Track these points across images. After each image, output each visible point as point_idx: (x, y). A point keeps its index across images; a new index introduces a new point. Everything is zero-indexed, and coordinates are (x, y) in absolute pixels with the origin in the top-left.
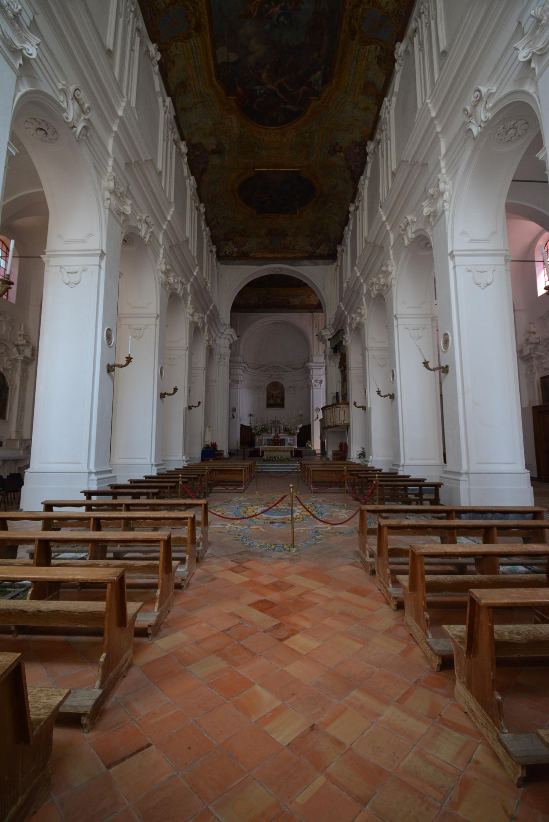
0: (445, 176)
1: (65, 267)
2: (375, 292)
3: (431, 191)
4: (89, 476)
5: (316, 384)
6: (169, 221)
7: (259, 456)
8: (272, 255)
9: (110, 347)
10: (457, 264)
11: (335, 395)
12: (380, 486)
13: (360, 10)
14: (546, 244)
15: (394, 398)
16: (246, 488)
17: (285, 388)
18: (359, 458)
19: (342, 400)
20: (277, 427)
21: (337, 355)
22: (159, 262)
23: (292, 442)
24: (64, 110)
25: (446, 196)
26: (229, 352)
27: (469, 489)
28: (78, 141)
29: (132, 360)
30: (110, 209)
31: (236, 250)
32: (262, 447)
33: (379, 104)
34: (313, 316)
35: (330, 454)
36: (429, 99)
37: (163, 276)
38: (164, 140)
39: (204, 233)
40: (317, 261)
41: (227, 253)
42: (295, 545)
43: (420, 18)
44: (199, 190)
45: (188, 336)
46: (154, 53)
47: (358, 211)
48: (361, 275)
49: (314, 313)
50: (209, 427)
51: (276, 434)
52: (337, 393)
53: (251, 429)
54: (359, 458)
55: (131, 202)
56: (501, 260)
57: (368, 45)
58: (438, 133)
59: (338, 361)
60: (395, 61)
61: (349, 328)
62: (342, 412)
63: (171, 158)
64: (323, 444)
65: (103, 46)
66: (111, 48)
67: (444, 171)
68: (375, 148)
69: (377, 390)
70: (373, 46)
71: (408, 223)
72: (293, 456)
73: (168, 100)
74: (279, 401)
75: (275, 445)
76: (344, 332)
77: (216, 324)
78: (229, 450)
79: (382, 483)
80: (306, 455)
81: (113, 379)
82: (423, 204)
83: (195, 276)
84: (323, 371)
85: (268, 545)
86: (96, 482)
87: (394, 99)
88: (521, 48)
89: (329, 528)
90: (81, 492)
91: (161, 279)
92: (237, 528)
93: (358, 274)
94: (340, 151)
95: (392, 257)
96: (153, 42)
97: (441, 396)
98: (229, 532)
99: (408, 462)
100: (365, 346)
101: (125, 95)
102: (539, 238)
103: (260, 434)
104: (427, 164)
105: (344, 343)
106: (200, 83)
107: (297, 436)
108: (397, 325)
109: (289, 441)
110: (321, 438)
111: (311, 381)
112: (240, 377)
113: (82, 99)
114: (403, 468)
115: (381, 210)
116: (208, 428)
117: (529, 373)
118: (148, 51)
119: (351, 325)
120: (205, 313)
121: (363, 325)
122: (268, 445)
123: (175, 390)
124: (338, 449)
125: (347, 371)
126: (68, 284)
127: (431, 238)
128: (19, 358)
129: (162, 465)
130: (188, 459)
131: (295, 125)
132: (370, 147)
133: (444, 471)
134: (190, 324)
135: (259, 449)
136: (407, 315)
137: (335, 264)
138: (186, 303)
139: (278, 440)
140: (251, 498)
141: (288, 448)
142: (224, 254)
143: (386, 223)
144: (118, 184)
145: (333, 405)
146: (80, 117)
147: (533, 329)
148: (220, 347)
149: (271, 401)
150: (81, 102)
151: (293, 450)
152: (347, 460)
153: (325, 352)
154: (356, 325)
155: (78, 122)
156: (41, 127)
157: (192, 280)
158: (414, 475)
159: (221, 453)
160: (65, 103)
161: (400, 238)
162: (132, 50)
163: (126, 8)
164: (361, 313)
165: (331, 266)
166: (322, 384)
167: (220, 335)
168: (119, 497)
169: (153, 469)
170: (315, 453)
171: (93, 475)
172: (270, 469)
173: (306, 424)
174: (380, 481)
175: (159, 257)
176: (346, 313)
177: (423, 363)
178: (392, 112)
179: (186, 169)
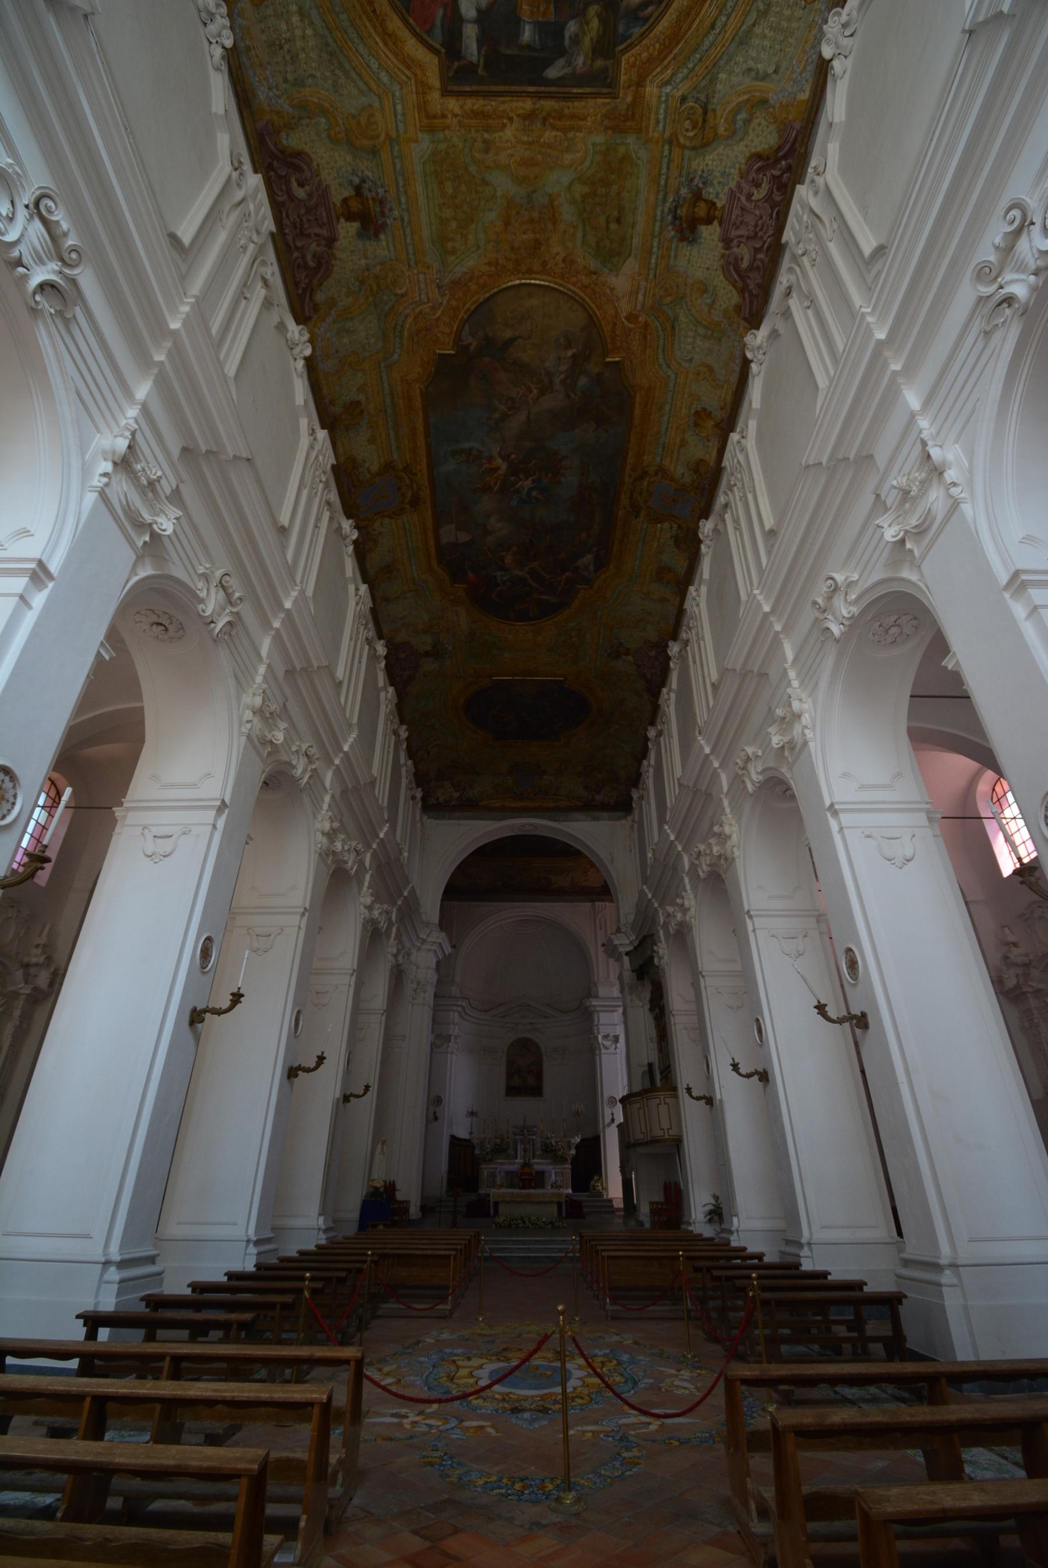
0: (799, 690)
1: (150, 827)
2: (754, 777)
3: (779, 712)
4: (104, 1271)
6: (288, 612)
8: (519, 804)
9: (204, 973)
11: (646, 1068)
12: (765, 1303)
13: (645, 483)
14: (994, 790)
15: (767, 1080)
19: (661, 1080)
22: (320, 818)
24: (201, 601)
25: (806, 719)
27: (965, 1308)
28: (215, 640)
29: (242, 999)
30: (249, 737)
31: (457, 795)
33: (683, 594)
35: (644, 1209)
37: (325, 840)
38: (351, 639)
39: (404, 770)
40: (597, 814)
41: (441, 800)
42: (573, 1480)
43: (731, 491)
44: (400, 707)
45: (357, 947)
46: (348, 531)
47: (662, 738)
48: (677, 838)
49: (597, 903)
50: (383, 1143)
52: (650, 1065)
53: (473, 1147)
54: (710, 1221)
55: (286, 725)
56: (922, 819)
57: (660, 523)
58: (777, 633)
59: (647, 995)
60: (700, 542)
61: (664, 934)
62: (663, 1108)
63: (360, 662)
65: (275, 521)
66: (286, 524)
67: (795, 684)
68: (681, 651)
69: (731, 1062)
70: (666, 525)
71: (748, 757)
72: (564, 1215)
73: (364, 588)
75: (523, 1187)
78: (422, 1200)
79: (767, 1295)
81: (197, 1038)
82: (770, 730)
83: (382, 840)
84: (617, 1016)
85: (505, 1481)
86: (116, 1286)
87: (704, 589)
88: (773, 733)
89: (653, 1427)
90: (78, 1317)
91: (319, 846)
92: (430, 1426)
93: (672, 837)
94: (627, 654)
95: (728, 810)
96: (348, 517)
97: (863, 1072)
98: (411, 1437)
99: (819, 1235)
100: (697, 968)
101: (298, 581)
102: (980, 778)
103: (491, 1160)
104: (711, 794)
105: (656, 960)
107: (572, 1164)
108: (754, 930)
109: (553, 1176)
111: (596, 1038)
113: (231, 587)
114: (811, 1250)
115: (700, 738)
116: (379, 1146)
117: (1026, 1025)
118: (340, 528)
120: (394, 903)
121: (690, 928)
122: (507, 1188)
123: (321, 1059)
126: (150, 856)
127: (792, 782)
128: (22, 991)
129: (268, 1240)
130: (331, 1224)
132: (674, 649)
133: (902, 1259)
134: (363, 924)
135: (488, 1195)
136: (769, 910)
137: (629, 818)
142: (435, 802)
143: (712, 757)
144: (269, 700)
145: (644, 1093)
146: (224, 609)
147: (1011, 938)
148: (418, 968)
150: (230, 591)
151: (563, 1200)
152: (683, 1227)
153: (620, 978)
154: (676, 927)
155: (219, 616)
156: (160, 621)
157: (374, 846)
158: (840, 1271)
159: (404, 1207)
160: (205, 592)
161: (738, 781)
162: (316, 526)
163: (314, 478)
164: (682, 905)
165: (623, 822)
166: (618, 1045)
168: (161, 1333)
170: (612, 1206)
171: (113, 1269)
174: (764, 1289)
175: (321, 808)
176: (656, 905)
177: (816, 1007)
178: (703, 605)
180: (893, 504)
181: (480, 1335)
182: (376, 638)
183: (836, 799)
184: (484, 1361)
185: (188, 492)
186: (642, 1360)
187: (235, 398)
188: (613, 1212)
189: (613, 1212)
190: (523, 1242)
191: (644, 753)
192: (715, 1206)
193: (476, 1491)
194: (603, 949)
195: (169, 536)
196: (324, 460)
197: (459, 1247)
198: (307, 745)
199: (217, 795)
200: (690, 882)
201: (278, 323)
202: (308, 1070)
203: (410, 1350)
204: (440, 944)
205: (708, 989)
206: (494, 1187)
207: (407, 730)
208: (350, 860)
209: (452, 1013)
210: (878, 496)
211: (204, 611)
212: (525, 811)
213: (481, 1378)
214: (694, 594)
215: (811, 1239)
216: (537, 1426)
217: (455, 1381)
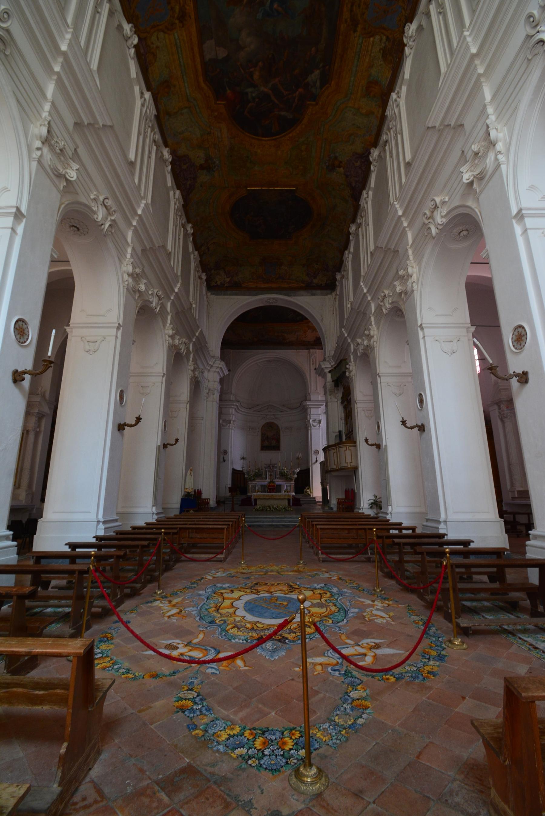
2: (388, 306)
3: (401, 272)
6: (140, 216)
7: (251, 504)
8: (267, 286)
10: (426, 334)
15: (424, 430)
16: (229, 553)
17: (281, 429)
18: (371, 508)
20: (273, 472)
21: (338, 390)
22: (125, 263)
23: (289, 489)
26: (219, 387)
28: (105, 236)
30: (127, 289)
31: (228, 280)
32: (254, 495)
34: (309, 352)
35: (334, 502)
36: (468, 31)
38: (173, 225)
40: (314, 292)
41: (219, 283)
48: (368, 291)
49: (311, 350)
50: (191, 470)
51: (271, 479)
52: (340, 432)
53: (244, 474)
54: (371, 508)
57: (372, 36)
58: (405, 228)
59: (340, 395)
60: (370, 163)
62: (348, 452)
64: (324, 491)
68: (356, 230)
70: (377, 37)
73: (178, 192)
75: (270, 492)
76: (347, 362)
77: (203, 354)
82: (395, 283)
83: (176, 293)
88: (464, 172)
90: (66, 544)
93: (365, 291)
96: (129, 22)
99: (452, 517)
101: (70, 20)
103: (253, 480)
104: (398, 251)
105: (347, 374)
106: (186, 84)
107: (295, 481)
109: (285, 487)
112: (233, 417)
116: (189, 472)
119: (357, 352)
122: (262, 492)
123: (177, 440)
124: (344, 497)
125: (352, 406)
129: (161, 513)
130: (161, 511)
131: (290, 135)
134: (191, 379)
135: (252, 496)
137: (334, 294)
139: (274, 486)
140: (232, 571)
141: (285, 495)
142: (216, 284)
143: (403, 219)
148: (209, 381)
151: (291, 498)
152: (356, 510)
153: (325, 387)
157: (172, 298)
159: (206, 502)
163: (145, 126)
164: (369, 335)
165: (329, 296)
166: (321, 425)
167: (209, 368)
168: (78, 561)
169: (98, 527)
170: (315, 500)
172: (263, 522)
173: (304, 468)
175: (126, 256)
178: (370, 203)
179: (134, 66)
180: (469, 159)
181: (241, 573)
182: (187, 223)
183: (424, 322)
184: (242, 593)
185: (82, 151)
186: (346, 593)
187: (99, 87)
189: (316, 503)
190: (269, 518)
191: (346, 246)
192: (374, 500)
193: (218, 751)
194: (315, 371)
195: (75, 181)
196: (150, 113)
197: (231, 523)
198: (157, 290)
199: (14, 203)
200: (374, 320)
201: (118, 25)
202: (172, 445)
203: (195, 585)
205: (382, 383)
206: (255, 492)
207: (206, 275)
208: (183, 349)
209: (231, 409)
210: (463, 152)
211: (97, 218)
212: (270, 290)
213: (239, 608)
214: (365, 196)
215: (447, 519)
216: (276, 658)
217: (220, 611)
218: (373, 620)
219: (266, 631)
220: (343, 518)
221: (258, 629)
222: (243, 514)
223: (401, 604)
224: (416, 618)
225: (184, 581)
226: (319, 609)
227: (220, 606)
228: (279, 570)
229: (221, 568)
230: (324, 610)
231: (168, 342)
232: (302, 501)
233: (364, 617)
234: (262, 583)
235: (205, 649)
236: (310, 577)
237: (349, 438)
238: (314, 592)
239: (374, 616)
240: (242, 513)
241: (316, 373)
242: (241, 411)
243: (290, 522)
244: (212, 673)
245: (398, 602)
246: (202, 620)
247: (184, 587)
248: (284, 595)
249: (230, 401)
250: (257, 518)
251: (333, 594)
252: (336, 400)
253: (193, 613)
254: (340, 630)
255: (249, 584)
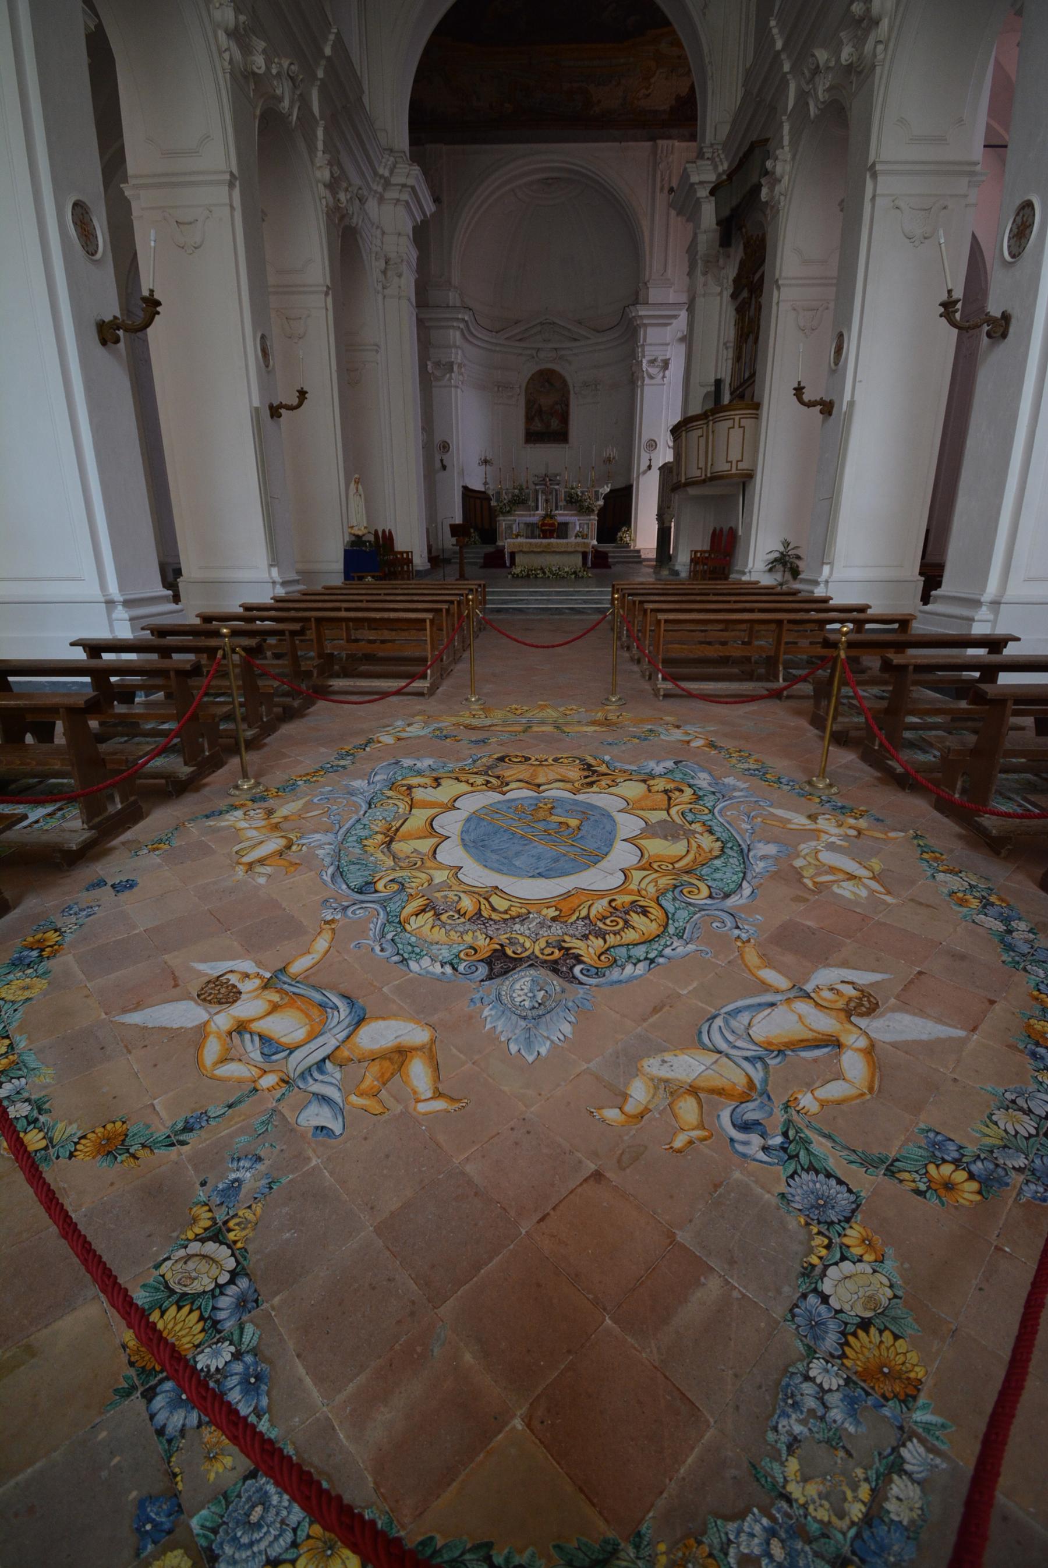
5: (653, 371)
9: (96, 262)
11: (713, 388)
16: (443, 674)
20: (551, 493)
21: (729, 257)
26: (414, 254)
29: (159, 309)
32: (508, 544)
34: (654, 152)
35: (682, 560)
49: (660, 142)
51: (546, 509)
52: (718, 383)
54: (770, 570)
59: (731, 272)
62: (736, 434)
64: (663, 535)
72: (589, 564)
74: (555, 424)
75: (545, 537)
80: (618, 562)
83: (329, 59)
103: (509, 512)
107: (598, 515)
110: (661, 517)
111: (640, 363)
116: (352, 486)
124: (707, 547)
125: (763, 300)
138: (312, 149)
139: (553, 525)
140: (446, 722)
141: (578, 544)
148: (383, 233)
149: (538, 426)
151: (589, 550)
152: (733, 576)
153: (691, 251)
157: (320, 74)
166: (667, 372)
167: (380, 189)
169: (114, 616)
172: (528, 602)
173: (620, 484)
177: (942, 304)
181: (469, 727)
184: (464, 787)
186: (735, 789)
188: (640, 562)
190: (542, 594)
192: (782, 553)
200: (790, 132)
204: (413, 188)
205: (878, 200)
209: (451, 331)
216: (543, 1051)
218: (827, 885)
219: (517, 927)
220: (714, 594)
221: (494, 916)
222: (480, 585)
223: (894, 830)
224: (955, 883)
225: (323, 750)
226: (666, 843)
227: (397, 830)
228: (560, 721)
229: (418, 714)
230: (678, 848)
231: (226, 56)
232: (614, 557)
233: (798, 875)
234: (516, 757)
235: (322, 1006)
236: (637, 741)
237: (742, 397)
238: (649, 786)
239: (827, 873)
240: (478, 582)
241: (671, 205)
242: (474, 336)
243: (585, 602)
244: (317, 1128)
245: (882, 821)
246: (340, 880)
247: (317, 767)
248: (573, 796)
249: (448, 307)
250: (516, 593)
251: (701, 793)
252: (719, 289)
253: (321, 852)
254: (737, 927)
255: (484, 760)
